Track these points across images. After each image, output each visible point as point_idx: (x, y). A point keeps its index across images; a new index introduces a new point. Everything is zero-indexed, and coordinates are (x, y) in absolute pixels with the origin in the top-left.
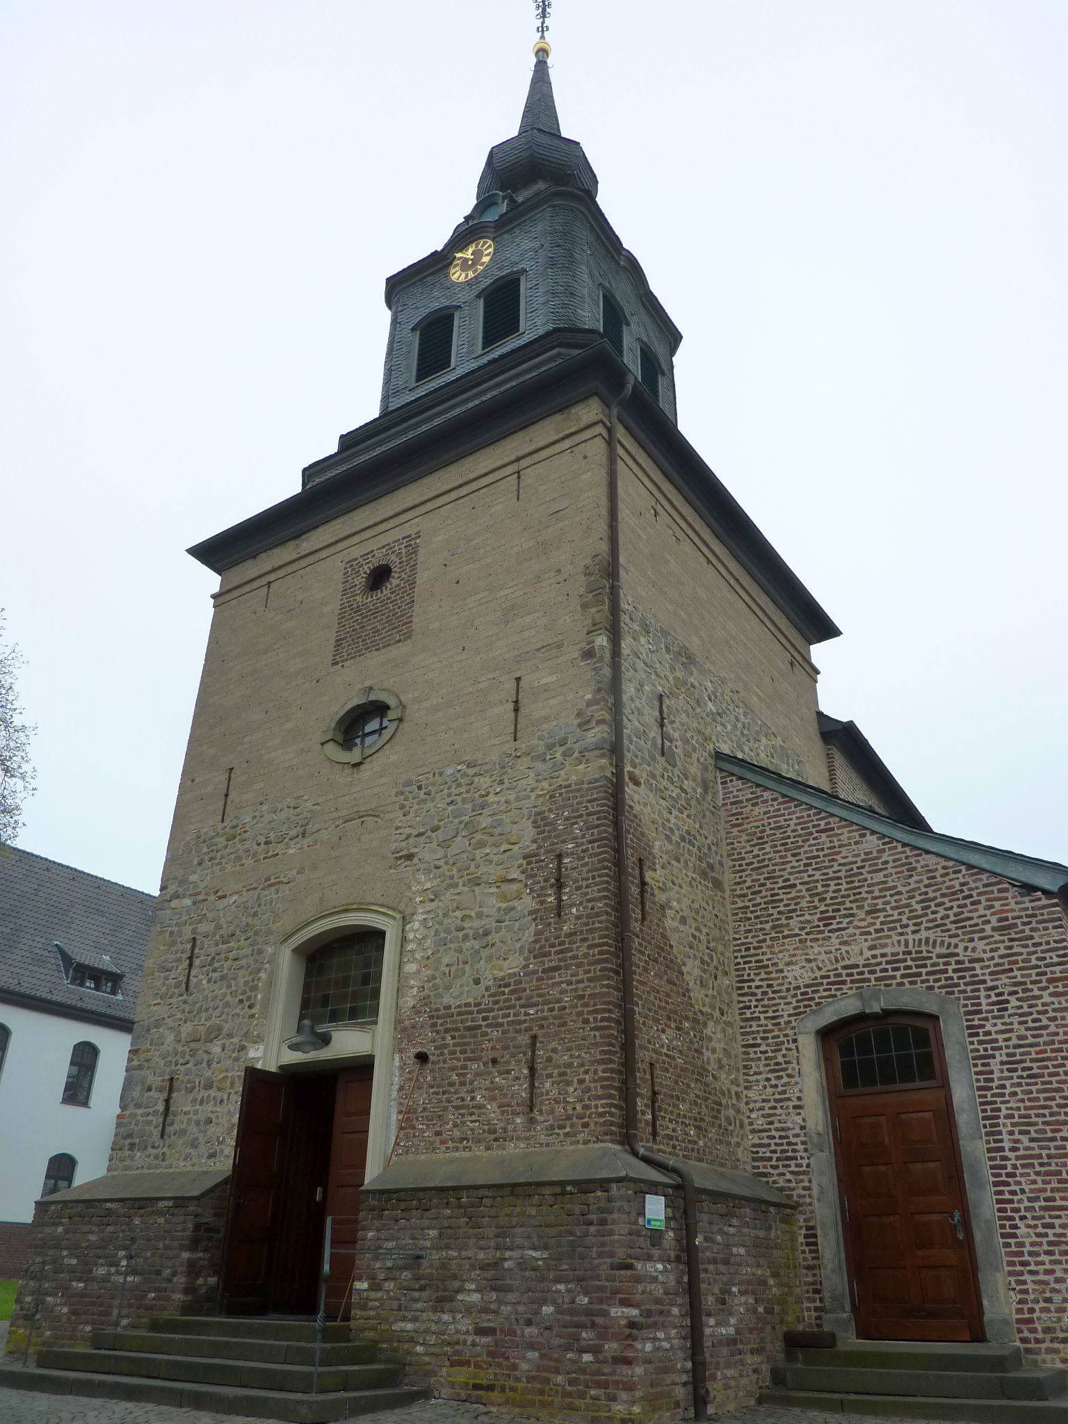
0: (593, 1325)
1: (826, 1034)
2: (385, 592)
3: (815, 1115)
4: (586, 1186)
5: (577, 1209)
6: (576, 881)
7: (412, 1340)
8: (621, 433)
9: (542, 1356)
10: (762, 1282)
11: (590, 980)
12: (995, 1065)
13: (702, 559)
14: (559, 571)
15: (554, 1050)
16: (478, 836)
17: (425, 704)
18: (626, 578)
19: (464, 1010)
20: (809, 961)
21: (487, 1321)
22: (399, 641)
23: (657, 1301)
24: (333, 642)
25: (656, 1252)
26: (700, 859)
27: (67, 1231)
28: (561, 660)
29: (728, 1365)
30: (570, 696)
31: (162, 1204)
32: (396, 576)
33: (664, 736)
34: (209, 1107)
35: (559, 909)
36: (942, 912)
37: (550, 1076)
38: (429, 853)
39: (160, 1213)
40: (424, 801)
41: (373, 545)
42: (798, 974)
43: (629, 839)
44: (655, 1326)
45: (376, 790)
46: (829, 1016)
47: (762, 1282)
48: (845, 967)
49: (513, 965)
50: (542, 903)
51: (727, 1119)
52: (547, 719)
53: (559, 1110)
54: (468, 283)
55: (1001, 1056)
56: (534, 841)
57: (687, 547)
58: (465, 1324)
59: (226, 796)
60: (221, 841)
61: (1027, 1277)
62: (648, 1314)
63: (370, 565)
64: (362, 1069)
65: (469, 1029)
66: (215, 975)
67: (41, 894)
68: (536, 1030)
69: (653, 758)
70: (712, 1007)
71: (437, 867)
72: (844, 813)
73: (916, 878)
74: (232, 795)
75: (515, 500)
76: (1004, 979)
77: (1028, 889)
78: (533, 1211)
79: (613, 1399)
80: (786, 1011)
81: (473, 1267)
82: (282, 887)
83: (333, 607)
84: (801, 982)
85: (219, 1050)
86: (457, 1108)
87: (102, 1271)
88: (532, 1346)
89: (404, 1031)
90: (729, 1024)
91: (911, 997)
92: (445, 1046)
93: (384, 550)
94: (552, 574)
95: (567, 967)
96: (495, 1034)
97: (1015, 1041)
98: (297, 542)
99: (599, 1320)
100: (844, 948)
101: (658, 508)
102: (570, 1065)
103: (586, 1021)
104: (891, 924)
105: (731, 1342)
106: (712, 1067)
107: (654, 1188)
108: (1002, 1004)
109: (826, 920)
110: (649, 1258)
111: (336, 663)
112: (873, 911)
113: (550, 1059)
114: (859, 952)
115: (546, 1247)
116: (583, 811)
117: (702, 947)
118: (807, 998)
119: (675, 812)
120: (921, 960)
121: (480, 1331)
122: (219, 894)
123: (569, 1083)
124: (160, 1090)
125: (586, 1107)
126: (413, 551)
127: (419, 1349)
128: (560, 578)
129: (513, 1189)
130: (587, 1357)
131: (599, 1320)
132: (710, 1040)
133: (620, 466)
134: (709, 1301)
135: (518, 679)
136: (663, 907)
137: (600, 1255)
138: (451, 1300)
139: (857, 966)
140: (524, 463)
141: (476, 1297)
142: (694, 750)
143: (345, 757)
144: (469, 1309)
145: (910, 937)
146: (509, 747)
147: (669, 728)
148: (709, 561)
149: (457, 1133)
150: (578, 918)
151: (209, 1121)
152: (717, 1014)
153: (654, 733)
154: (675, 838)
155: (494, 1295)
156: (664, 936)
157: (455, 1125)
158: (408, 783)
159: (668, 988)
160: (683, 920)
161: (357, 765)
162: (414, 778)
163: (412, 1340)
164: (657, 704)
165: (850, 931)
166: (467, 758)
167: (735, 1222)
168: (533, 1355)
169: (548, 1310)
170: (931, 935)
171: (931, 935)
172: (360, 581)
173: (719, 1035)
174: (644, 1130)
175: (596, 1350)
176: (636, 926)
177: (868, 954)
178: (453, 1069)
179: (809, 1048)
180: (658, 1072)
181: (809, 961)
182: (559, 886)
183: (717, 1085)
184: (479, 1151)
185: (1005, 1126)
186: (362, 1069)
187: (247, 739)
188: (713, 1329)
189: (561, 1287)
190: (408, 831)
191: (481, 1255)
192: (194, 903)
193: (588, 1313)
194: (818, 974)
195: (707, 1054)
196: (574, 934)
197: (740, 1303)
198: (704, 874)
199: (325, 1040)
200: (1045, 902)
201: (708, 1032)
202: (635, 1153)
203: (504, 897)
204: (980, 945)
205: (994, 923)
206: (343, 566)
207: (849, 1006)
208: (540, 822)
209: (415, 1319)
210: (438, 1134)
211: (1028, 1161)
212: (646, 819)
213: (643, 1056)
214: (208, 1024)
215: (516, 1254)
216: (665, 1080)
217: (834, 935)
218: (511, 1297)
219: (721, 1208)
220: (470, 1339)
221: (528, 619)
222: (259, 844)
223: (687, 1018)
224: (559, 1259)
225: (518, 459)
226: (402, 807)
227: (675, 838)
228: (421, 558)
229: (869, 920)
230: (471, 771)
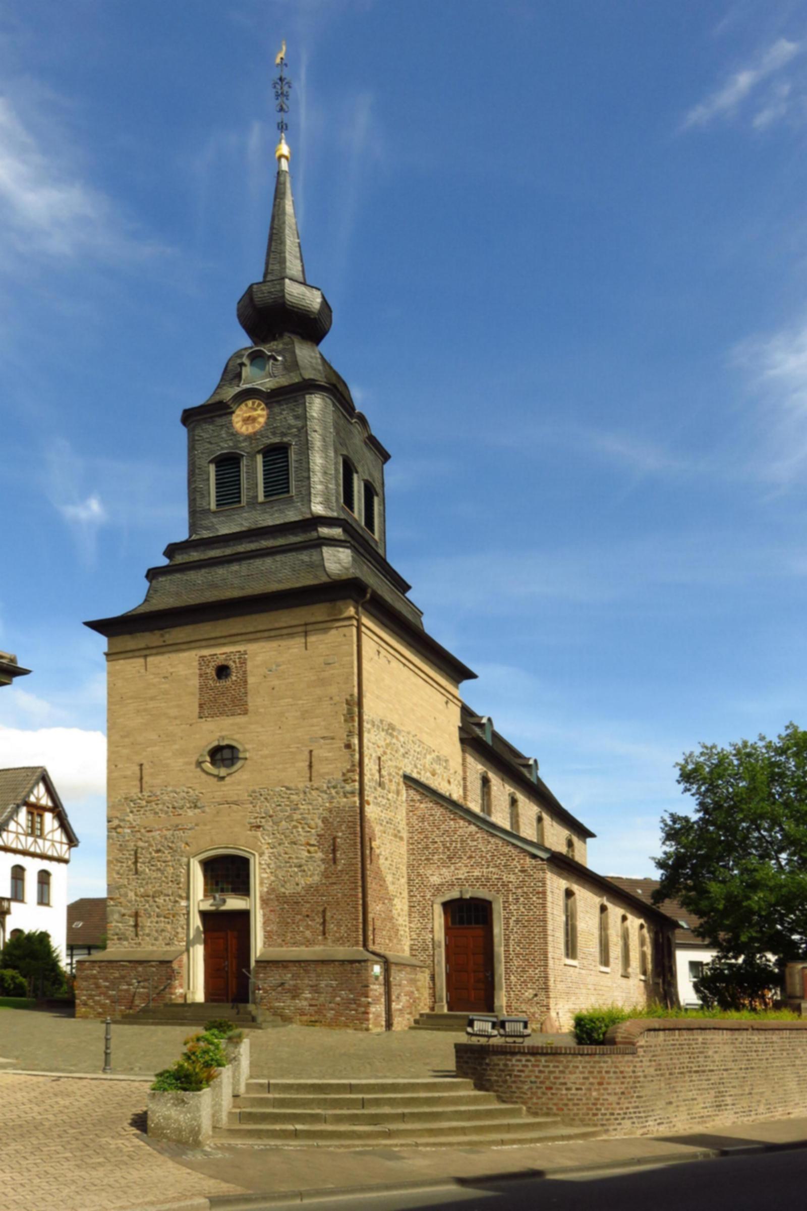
0: (355, 1003)
1: (446, 905)
3: (440, 935)
4: (352, 962)
5: (349, 968)
6: (343, 849)
7: (283, 1009)
8: (365, 620)
9: (337, 1012)
10: (412, 992)
11: (350, 889)
12: (511, 921)
13: (401, 666)
14: (331, 698)
15: (335, 914)
16: (294, 823)
17: (260, 753)
18: (365, 701)
19: (292, 895)
20: (441, 875)
21: (314, 1002)
22: (240, 714)
23: (377, 997)
24: (196, 705)
25: (377, 982)
26: (394, 829)
27: (99, 972)
28: (334, 746)
29: (399, 1017)
30: (339, 765)
31: (153, 963)
33: (381, 776)
34: (162, 925)
35: (335, 860)
36: (499, 861)
37: (333, 923)
38: (268, 825)
39: (153, 966)
40: (263, 802)
41: (218, 651)
42: (435, 880)
43: (367, 830)
44: (376, 1004)
45: (236, 792)
46: (447, 897)
47: (412, 992)
48: (456, 879)
49: (316, 878)
50: (327, 856)
51: (401, 936)
52: (328, 774)
53: (337, 935)
54: (250, 438)
55: (514, 918)
56: (323, 829)
57: (395, 663)
58: (305, 1003)
59: (141, 779)
60: (144, 803)
61: (512, 993)
62: (374, 1000)
64: (244, 916)
65: (295, 903)
66: (153, 868)
67: (631, 1080)
68: (326, 905)
69: (375, 789)
70: (397, 892)
71: (273, 834)
72: (462, 814)
73: (490, 846)
74: (145, 779)
75: (304, 649)
76: (520, 890)
77: (534, 857)
78: (331, 969)
79: (362, 1023)
80: (428, 896)
81: (307, 986)
82: (186, 831)
83: (195, 682)
84: (436, 883)
85: (162, 901)
86: (292, 932)
87: (125, 987)
88: (332, 1009)
89: (265, 902)
90: (403, 898)
91: (482, 893)
92: (285, 908)
94: (328, 699)
95: (340, 883)
96: (308, 905)
97: (520, 913)
98: (161, 632)
99: (358, 1002)
100: (456, 871)
101: (381, 650)
102: (341, 920)
103: (348, 904)
104: (479, 864)
105: (400, 1010)
106: (396, 916)
107: (377, 963)
108: (517, 899)
109: (450, 858)
110: (374, 984)
111: (201, 718)
112: (470, 857)
113: (332, 917)
114: (462, 874)
115: (336, 980)
116: (346, 820)
117: (394, 868)
118: (438, 889)
119: (384, 811)
120: (488, 880)
121: (311, 1005)
122: (148, 829)
123: (341, 926)
124: (130, 916)
125: (348, 935)
126: (243, 662)
127: (287, 1011)
128: (332, 702)
129: (323, 962)
130: (353, 1012)
131: (358, 1002)
132: (395, 905)
133: (364, 637)
134: (394, 997)
135: (311, 752)
136: (378, 856)
137: (358, 983)
138: (298, 996)
139: (460, 879)
140: (309, 628)
141: (309, 996)
142: (394, 777)
143: (215, 771)
144: (306, 999)
145: (485, 870)
146: (308, 784)
147: (384, 772)
148: (405, 665)
149: (292, 941)
150: (344, 864)
151: (163, 931)
152: (398, 895)
153: (377, 776)
154: (384, 823)
155: (316, 995)
156: (379, 868)
157: (291, 938)
158: (254, 792)
159: (379, 888)
160: (386, 859)
161: (222, 778)
162: (257, 790)
163: (283, 1009)
164: (377, 761)
165: (460, 864)
166: (286, 784)
167: (403, 972)
168: (333, 1012)
169: (338, 999)
170: (493, 870)
171: (493, 870)
172: (211, 671)
173: (399, 903)
174: (370, 942)
175: (356, 1010)
176: (368, 866)
177: (466, 875)
178: (289, 917)
179: (438, 910)
180: (375, 921)
181: (441, 875)
182: (334, 851)
183: (397, 922)
184: (303, 948)
185: (512, 942)
186: (244, 916)
187: (149, 749)
188: (394, 1006)
189: (343, 992)
190: (256, 815)
191: (310, 983)
192: (132, 832)
193: (354, 1000)
194: (444, 880)
195: (394, 911)
196: (342, 871)
197: (404, 999)
198: (396, 836)
199: (224, 901)
200: (540, 862)
201: (394, 902)
202: (368, 950)
203: (309, 852)
204: (512, 876)
205: (519, 868)
206: (197, 658)
207: (455, 894)
208: (325, 820)
209: (284, 1002)
210: (283, 941)
211: (517, 955)
212: (372, 819)
213: (370, 916)
214: (154, 889)
215: (324, 982)
216: (378, 923)
217: (452, 866)
218: (323, 995)
219: (399, 968)
220: (307, 1008)
221: (315, 720)
222: (168, 807)
223: (386, 899)
224: (342, 984)
225: (306, 624)
226: (252, 803)
227: (384, 823)
228: (249, 668)
229: (468, 861)
230: (289, 792)
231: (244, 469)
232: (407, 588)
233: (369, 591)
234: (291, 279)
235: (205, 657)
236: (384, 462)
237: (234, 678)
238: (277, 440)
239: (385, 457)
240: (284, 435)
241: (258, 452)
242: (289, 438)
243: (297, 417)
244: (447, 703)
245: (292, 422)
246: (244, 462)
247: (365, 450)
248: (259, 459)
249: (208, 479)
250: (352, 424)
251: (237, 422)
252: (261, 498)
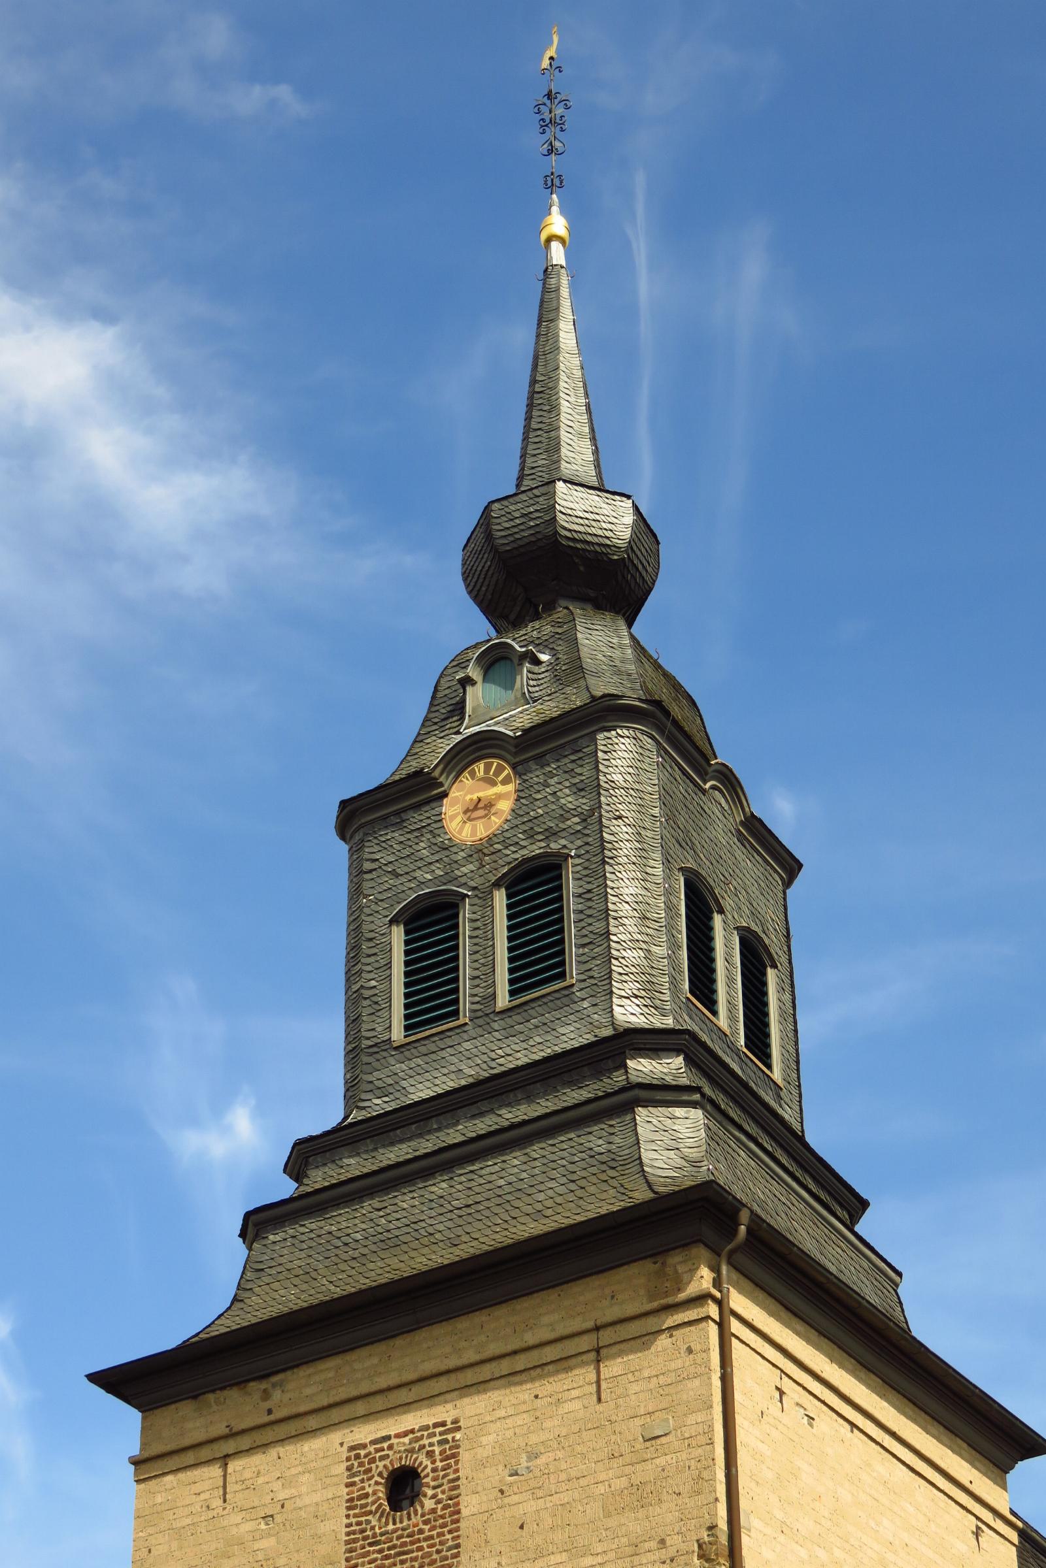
2: (412, 1520)
14: (662, 1541)
32: (430, 1492)
54: (479, 851)
57: (826, 1423)
63: (387, 1462)
93: (406, 1440)
98: (264, 1385)
140: (606, 1336)
172: (377, 1490)
231: (465, 930)
232: (854, 1205)
233: (744, 1216)
234: (565, 481)
235: (364, 1446)
236: (788, 883)
237: (429, 1504)
238: (536, 849)
239: (790, 867)
240: (551, 834)
241: (497, 885)
242: (563, 842)
243: (579, 790)
244: (977, 1533)
245: (569, 800)
246: (466, 912)
247: (740, 853)
248: (500, 899)
249: (389, 965)
250: (704, 792)
251: (453, 818)
252: (503, 1000)
